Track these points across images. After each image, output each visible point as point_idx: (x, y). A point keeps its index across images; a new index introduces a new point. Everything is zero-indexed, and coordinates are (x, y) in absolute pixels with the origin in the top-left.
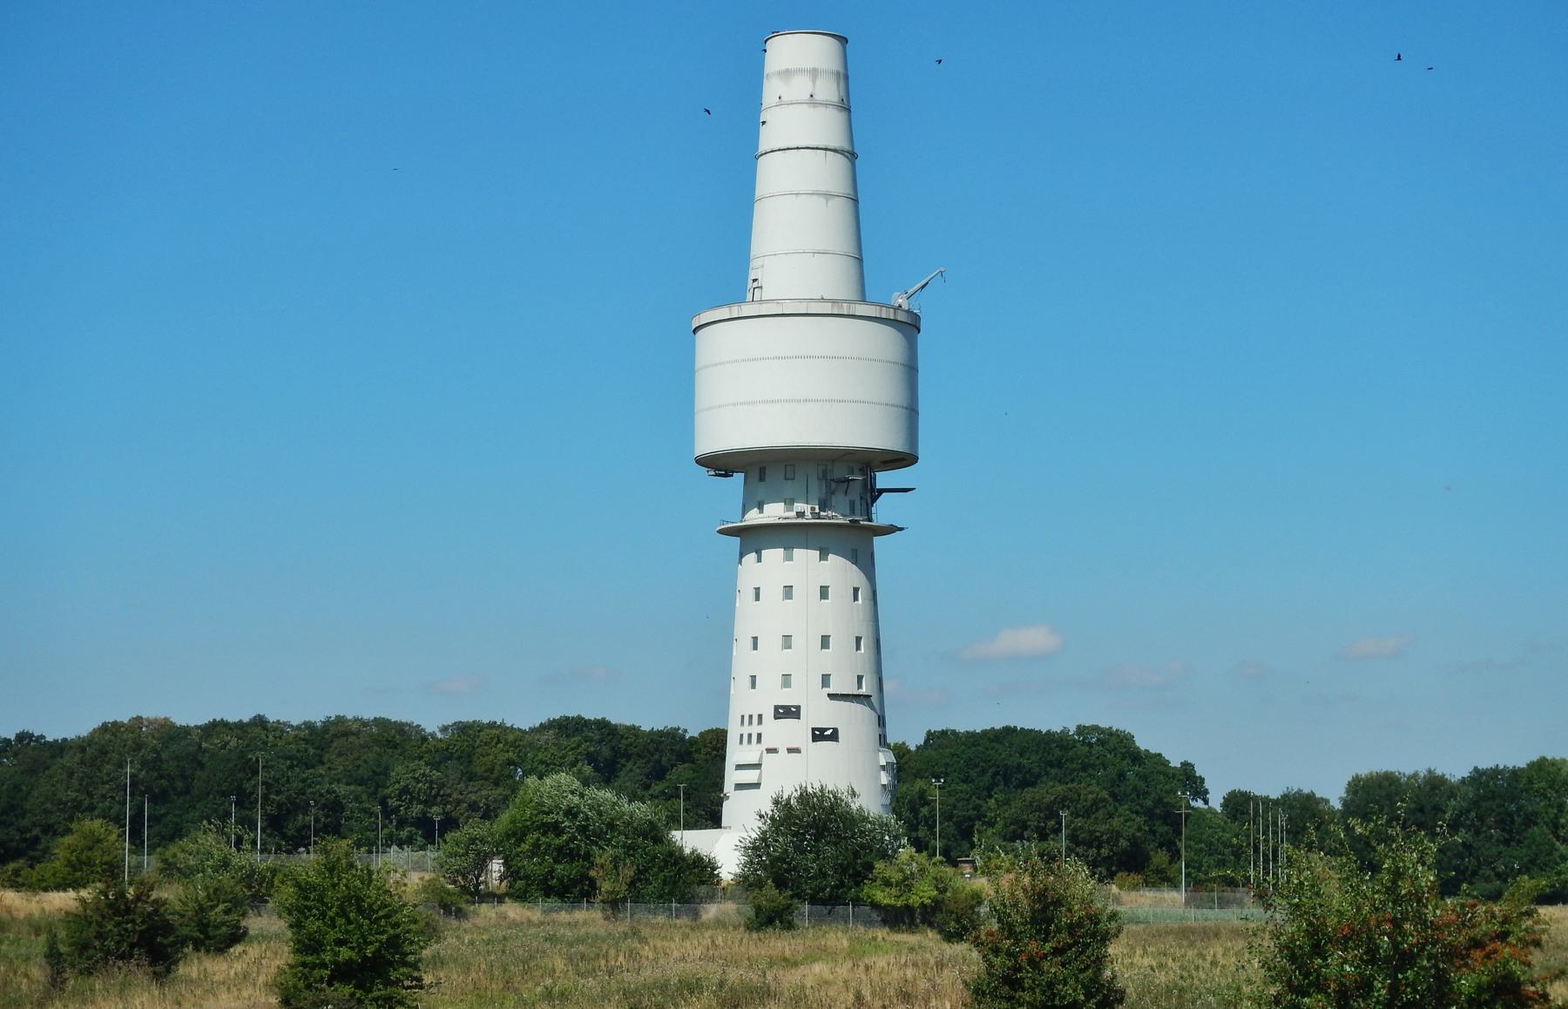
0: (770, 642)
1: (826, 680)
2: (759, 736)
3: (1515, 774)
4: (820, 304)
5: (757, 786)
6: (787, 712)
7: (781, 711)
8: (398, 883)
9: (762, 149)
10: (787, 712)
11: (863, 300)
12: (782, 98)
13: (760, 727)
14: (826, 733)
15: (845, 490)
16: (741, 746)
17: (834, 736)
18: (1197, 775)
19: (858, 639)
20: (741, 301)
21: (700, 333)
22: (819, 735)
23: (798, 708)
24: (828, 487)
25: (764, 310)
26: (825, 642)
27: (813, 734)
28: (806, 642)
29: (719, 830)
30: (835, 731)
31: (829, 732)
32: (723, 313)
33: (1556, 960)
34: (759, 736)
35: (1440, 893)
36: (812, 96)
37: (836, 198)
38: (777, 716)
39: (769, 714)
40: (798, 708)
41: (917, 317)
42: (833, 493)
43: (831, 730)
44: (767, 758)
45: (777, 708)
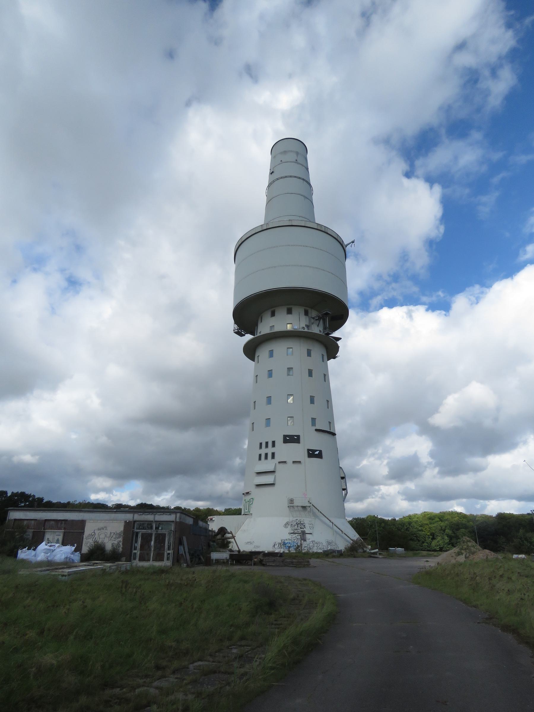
1: (314, 420)
3: (363, 519)
5: (273, 484)
8: (119, 577)
13: (274, 448)
14: (315, 453)
15: (317, 325)
16: (260, 461)
17: (320, 456)
18: (210, 529)
20: (34, 531)
22: (312, 454)
23: (298, 436)
24: (310, 321)
26: (312, 400)
27: (309, 453)
29: (240, 516)
30: (320, 452)
31: (317, 453)
34: (273, 455)
39: (279, 441)
40: (298, 436)
42: (313, 324)
43: (318, 452)
44: (280, 467)
45: (285, 436)
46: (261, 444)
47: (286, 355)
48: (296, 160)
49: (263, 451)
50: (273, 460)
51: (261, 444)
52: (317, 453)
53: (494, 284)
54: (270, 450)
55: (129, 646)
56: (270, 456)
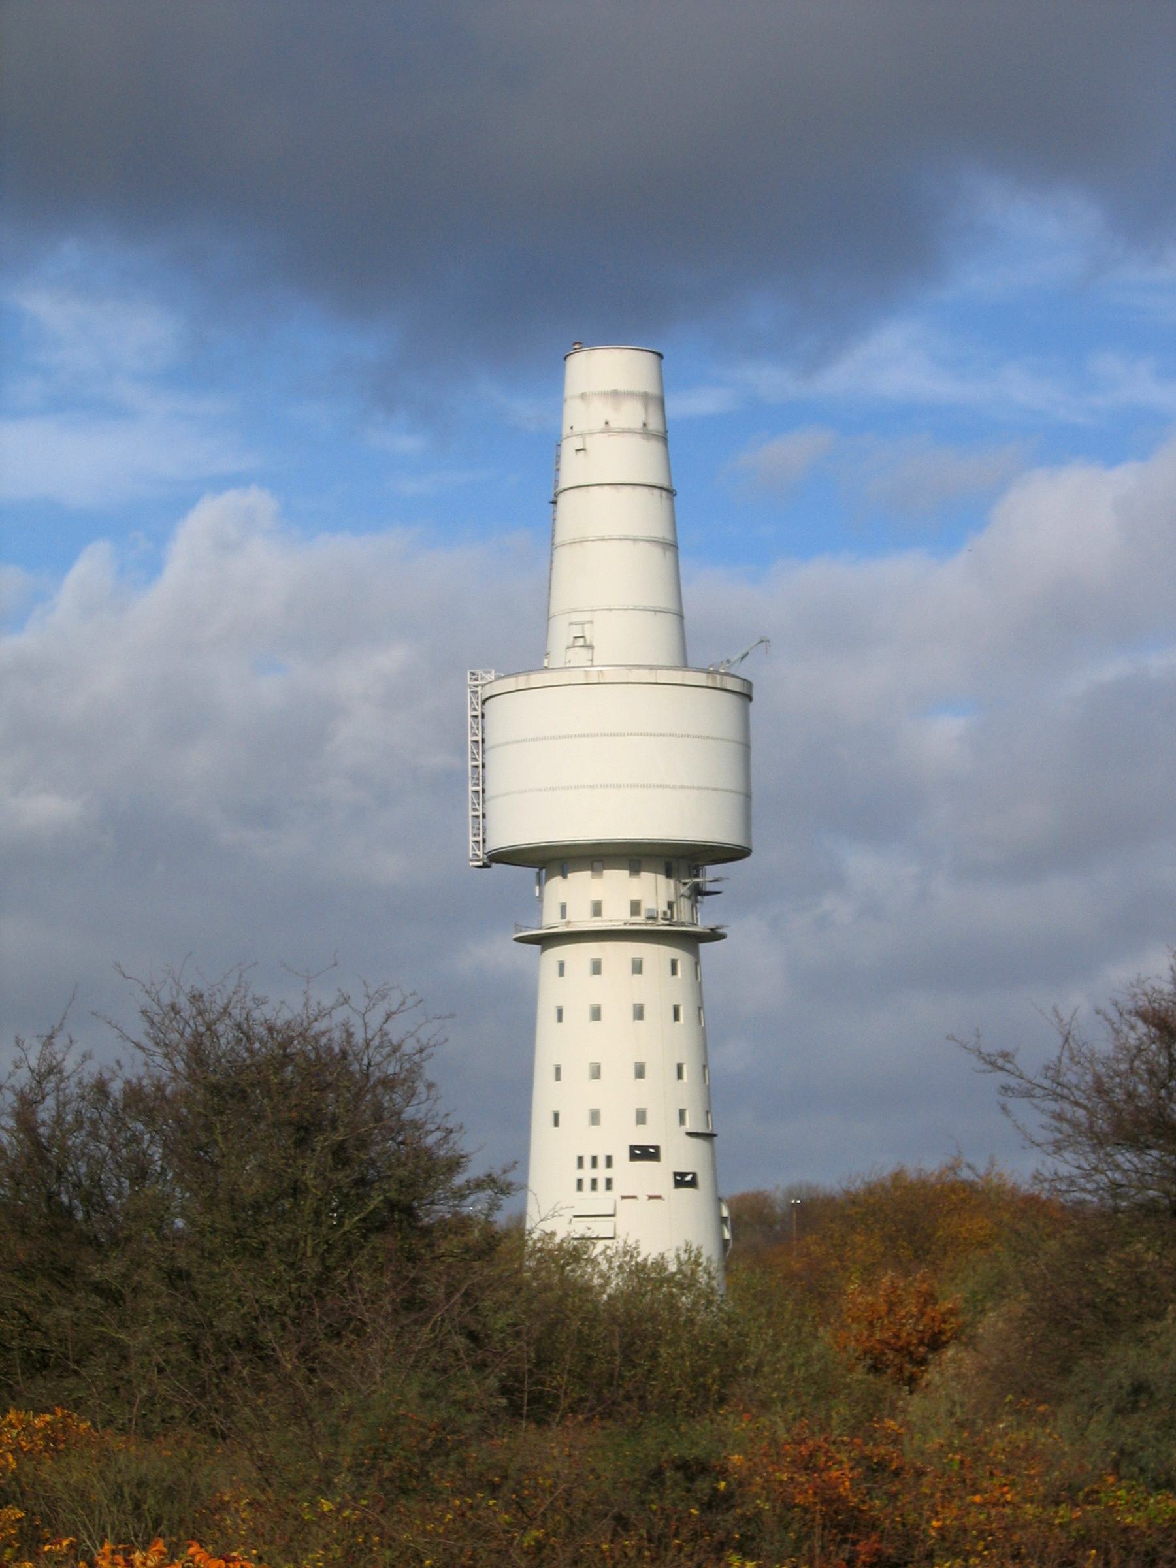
0: (577, 1072)
2: (609, 1182)
4: (672, 672)
6: (644, 1153)
7: (638, 1152)
9: (562, 486)
10: (644, 1153)
11: (685, 666)
12: (610, 423)
17: (693, 1184)
19: (680, 1068)
21: (488, 703)
25: (564, 677)
26: (640, 1072)
28: (618, 1071)
30: (694, 1175)
31: (688, 1178)
32: (521, 682)
33: (42, 1566)
34: (609, 1182)
35: (513, 1415)
36: (607, 423)
37: (641, 543)
38: (633, 1157)
40: (657, 1148)
41: (749, 684)
45: (632, 1148)
46: (580, 1159)
47: (566, 966)
48: (607, 423)
49: (587, 1174)
50: (608, 1193)
51: (580, 1159)
52: (688, 1178)
53: (649, 871)
54: (602, 1173)
55: (1051, 1543)
56: (601, 1184)
